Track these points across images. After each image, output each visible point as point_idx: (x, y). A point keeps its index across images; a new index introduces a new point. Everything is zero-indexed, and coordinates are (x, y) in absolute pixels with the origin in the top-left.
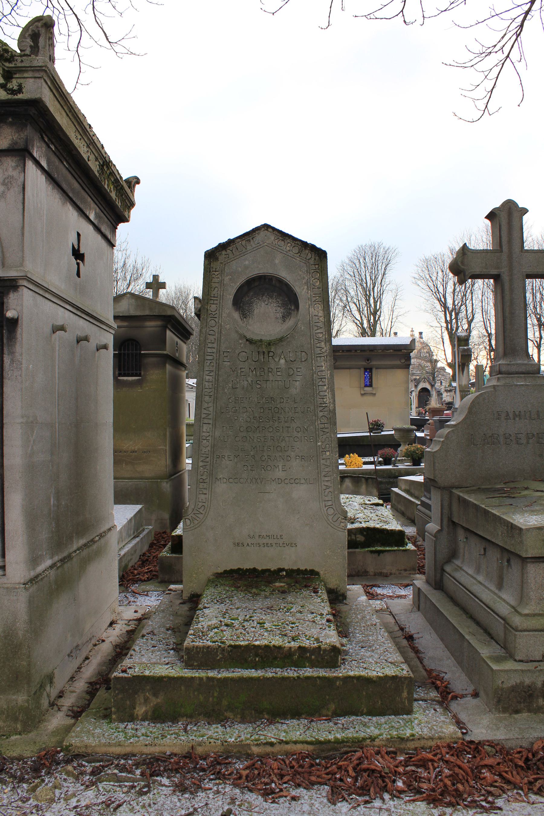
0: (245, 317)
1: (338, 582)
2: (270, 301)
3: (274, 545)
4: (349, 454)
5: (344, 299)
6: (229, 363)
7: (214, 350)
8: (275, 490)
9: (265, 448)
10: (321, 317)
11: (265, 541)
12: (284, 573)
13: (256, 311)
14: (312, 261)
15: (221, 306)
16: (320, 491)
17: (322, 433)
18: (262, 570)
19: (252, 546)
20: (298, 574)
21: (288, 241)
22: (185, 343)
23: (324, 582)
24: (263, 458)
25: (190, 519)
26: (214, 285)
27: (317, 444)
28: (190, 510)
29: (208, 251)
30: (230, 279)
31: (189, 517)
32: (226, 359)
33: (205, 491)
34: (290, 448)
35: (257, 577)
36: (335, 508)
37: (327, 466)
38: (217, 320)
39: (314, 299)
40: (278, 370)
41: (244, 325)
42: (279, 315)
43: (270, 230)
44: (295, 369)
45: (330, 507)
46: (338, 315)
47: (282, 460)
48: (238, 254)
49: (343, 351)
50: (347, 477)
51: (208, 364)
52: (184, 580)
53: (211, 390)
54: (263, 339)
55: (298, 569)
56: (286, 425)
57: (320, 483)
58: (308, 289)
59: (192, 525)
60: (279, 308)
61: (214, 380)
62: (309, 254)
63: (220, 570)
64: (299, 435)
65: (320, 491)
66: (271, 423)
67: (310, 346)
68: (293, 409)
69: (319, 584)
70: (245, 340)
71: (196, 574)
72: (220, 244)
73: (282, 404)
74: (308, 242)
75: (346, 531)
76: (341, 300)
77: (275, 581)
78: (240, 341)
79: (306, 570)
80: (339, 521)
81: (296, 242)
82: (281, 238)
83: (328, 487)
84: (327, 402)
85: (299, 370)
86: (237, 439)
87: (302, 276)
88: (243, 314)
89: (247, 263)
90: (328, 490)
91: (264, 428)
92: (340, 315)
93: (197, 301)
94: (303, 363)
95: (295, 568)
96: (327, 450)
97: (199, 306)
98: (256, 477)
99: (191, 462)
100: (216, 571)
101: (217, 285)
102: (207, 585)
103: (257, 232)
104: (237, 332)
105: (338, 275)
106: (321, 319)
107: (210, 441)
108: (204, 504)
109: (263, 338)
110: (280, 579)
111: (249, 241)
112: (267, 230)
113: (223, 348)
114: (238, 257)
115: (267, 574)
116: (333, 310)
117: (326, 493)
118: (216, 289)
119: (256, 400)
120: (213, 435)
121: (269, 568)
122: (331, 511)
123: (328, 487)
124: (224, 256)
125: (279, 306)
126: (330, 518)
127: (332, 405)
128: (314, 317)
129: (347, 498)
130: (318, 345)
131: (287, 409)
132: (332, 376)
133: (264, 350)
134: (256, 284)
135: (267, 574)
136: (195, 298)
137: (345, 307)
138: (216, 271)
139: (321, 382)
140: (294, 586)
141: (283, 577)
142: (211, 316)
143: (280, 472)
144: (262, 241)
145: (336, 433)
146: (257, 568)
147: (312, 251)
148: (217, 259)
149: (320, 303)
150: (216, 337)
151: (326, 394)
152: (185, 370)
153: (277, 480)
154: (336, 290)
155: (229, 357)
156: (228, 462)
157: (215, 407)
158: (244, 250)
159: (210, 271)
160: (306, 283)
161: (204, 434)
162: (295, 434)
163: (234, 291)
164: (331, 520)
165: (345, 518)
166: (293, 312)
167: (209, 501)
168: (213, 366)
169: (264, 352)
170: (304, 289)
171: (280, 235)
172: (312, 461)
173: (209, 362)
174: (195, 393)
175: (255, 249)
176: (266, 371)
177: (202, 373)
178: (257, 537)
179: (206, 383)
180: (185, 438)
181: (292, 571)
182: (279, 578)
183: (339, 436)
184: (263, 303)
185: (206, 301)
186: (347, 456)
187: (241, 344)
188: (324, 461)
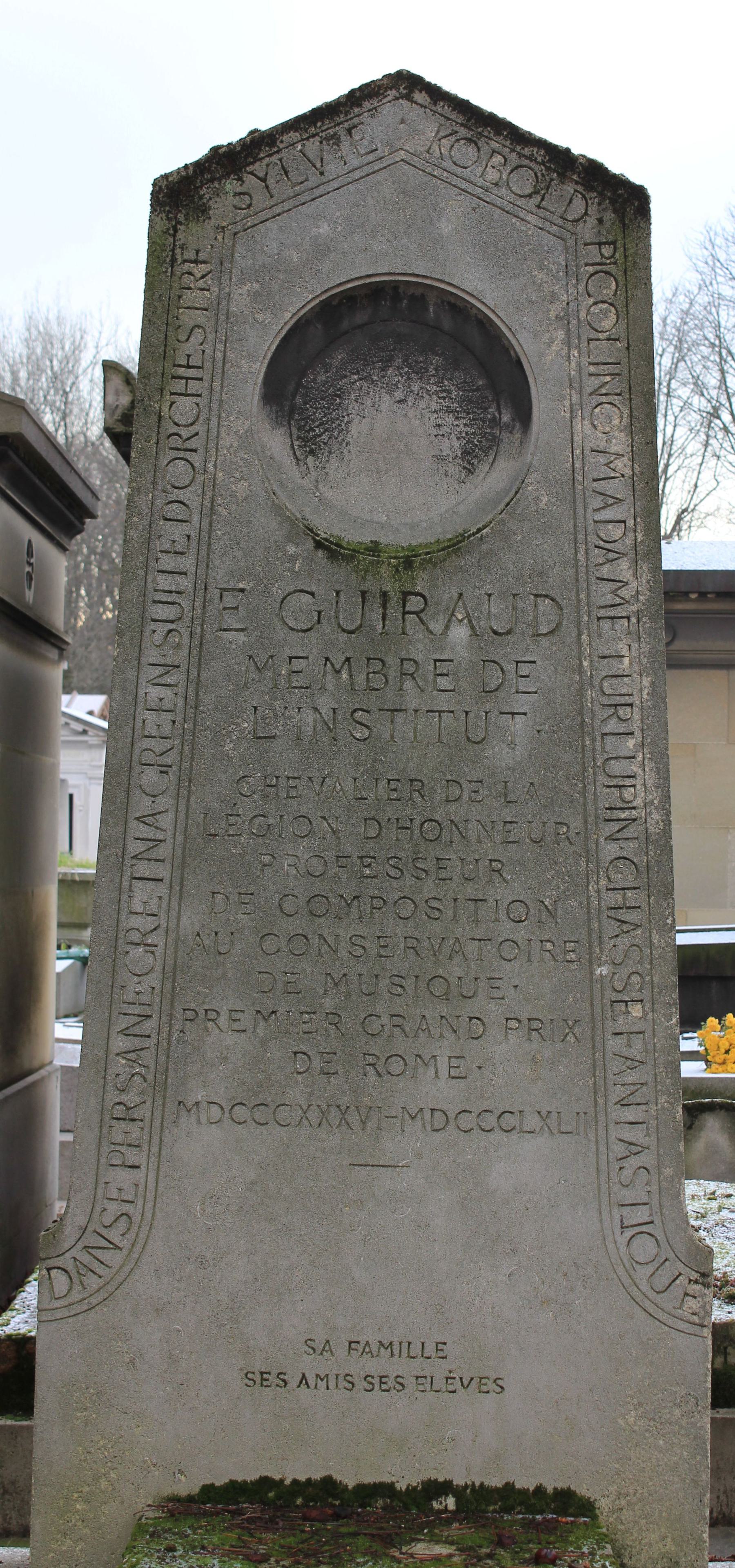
0: (312, 452)
1: (670, 1547)
2: (416, 387)
3: (410, 1382)
4: (720, 1017)
5: (712, 380)
6: (242, 637)
7: (185, 583)
8: (419, 1155)
9: (384, 983)
10: (619, 455)
11: (374, 1367)
12: (451, 1502)
13: (357, 429)
14: (588, 230)
15: (215, 405)
16: (603, 1166)
17: (612, 928)
18: (361, 1488)
19: (322, 1385)
20: (507, 1510)
21: (495, 145)
22: (63, 548)
23: (612, 1542)
24: (375, 1027)
25: (70, 1267)
26: (188, 318)
27: (592, 973)
28: (70, 1233)
29: (165, 177)
30: (255, 296)
31: (66, 1262)
32: (231, 621)
33: (132, 1156)
34: (483, 983)
35: (336, 1517)
36: (661, 1237)
37: (635, 1064)
38: (196, 459)
39: (595, 382)
40: (443, 668)
41: (307, 483)
42: (452, 446)
43: (420, 97)
44: (510, 668)
45: (642, 1229)
46: (683, 448)
47: (451, 1036)
48: (290, 193)
49: (703, 595)
50: (711, 1108)
51: (158, 638)
52: (36, 1524)
53: (167, 744)
54: (383, 540)
55: (509, 1487)
56: (470, 890)
57: (602, 1132)
58: (568, 343)
59: (75, 1296)
60: (450, 419)
61: (180, 703)
62: (578, 202)
63: (187, 1486)
64: (521, 933)
65: (603, 1166)
66: (409, 881)
67: (571, 572)
68: (500, 827)
69: (592, 1554)
70: (310, 544)
71: (87, 1501)
72: (215, 150)
73: (452, 807)
74: (576, 151)
75: (707, 1333)
76: (699, 388)
77: (413, 1533)
78: (291, 549)
79: (539, 1490)
80: (677, 1290)
81: (527, 151)
82: (463, 132)
83: (634, 1149)
84: (638, 802)
85: (524, 669)
86: (269, 945)
87: (547, 289)
88: (305, 440)
89: (324, 229)
90: (634, 1162)
91: (377, 903)
92: (694, 446)
93: (117, 381)
94: (544, 642)
95: (496, 1482)
96: (635, 995)
97: (125, 400)
98: (344, 1101)
99: (76, 1033)
100: (167, 1491)
101: (200, 317)
102: (130, 1549)
103: (367, 105)
104: (278, 510)
105: (692, 280)
106: (619, 464)
107: (159, 951)
108: (126, 1208)
109: (384, 539)
110: (430, 1525)
111: (335, 139)
112: (408, 97)
113: (220, 575)
114: (287, 206)
115: (380, 1503)
116: (664, 427)
117: (627, 1173)
118: (198, 335)
119: (349, 785)
120: (172, 925)
121: (387, 1479)
122: (645, 1248)
123: (634, 1149)
124: (231, 200)
125: (449, 411)
126: (643, 1273)
127: (656, 816)
128: (591, 458)
129: (712, 1196)
130: (605, 571)
131: (473, 825)
132: (659, 697)
133: (388, 587)
134: (361, 317)
135: (380, 1503)
136: (109, 367)
137: (715, 414)
138: (196, 262)
139: (613, 722)
140: (490, 1556)
141: (445, 1519)
142: (175, 441)
143: (442, 1083)
144: (388, 144)
145: (672, 929)
146: (337, 1477)
147: (589, 188)
148: (203, 211)
149: (616, 399)
150: (192, 529)
151: (635, 768)
152: (61, 657)
153: (427, 1115)
154: (679, 349)
155: (242, 611)
156: (230, 1039)
157: (182, 815)
158: (314, 180)
159: (173, 260)
160: (564, 319)
161: (135, 922)
162: (506, 929)
163: (268, 345)
164: (645, 1287)
165: (704, 1276)
166: (505, 435)
167: (150, 1195)
168: (178, 646)
169: (384, 595)
170: (552, 341)
171: (460, 119)
172: (571, 1039)
173: (162, 628)
174: (100, 757)
175: (357, 174)
176: (393, 673)
177: (131, 674)
178: (341, 1351)
179: (151, 717)
180: (53, 934)
181: (482, 1493)
182: (428, 1524)
183: (682, 939)
184: (386, 397)
185: (155, 381)
186: (712, 1021)
187: (293, 559)
188: (621, 1040)
